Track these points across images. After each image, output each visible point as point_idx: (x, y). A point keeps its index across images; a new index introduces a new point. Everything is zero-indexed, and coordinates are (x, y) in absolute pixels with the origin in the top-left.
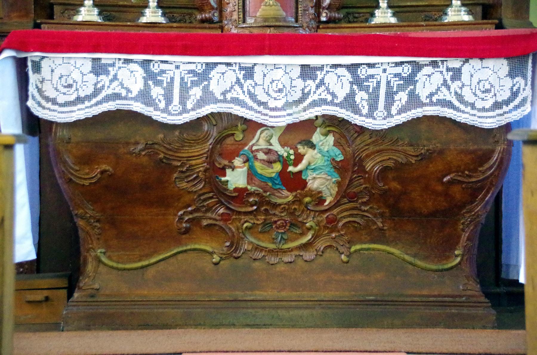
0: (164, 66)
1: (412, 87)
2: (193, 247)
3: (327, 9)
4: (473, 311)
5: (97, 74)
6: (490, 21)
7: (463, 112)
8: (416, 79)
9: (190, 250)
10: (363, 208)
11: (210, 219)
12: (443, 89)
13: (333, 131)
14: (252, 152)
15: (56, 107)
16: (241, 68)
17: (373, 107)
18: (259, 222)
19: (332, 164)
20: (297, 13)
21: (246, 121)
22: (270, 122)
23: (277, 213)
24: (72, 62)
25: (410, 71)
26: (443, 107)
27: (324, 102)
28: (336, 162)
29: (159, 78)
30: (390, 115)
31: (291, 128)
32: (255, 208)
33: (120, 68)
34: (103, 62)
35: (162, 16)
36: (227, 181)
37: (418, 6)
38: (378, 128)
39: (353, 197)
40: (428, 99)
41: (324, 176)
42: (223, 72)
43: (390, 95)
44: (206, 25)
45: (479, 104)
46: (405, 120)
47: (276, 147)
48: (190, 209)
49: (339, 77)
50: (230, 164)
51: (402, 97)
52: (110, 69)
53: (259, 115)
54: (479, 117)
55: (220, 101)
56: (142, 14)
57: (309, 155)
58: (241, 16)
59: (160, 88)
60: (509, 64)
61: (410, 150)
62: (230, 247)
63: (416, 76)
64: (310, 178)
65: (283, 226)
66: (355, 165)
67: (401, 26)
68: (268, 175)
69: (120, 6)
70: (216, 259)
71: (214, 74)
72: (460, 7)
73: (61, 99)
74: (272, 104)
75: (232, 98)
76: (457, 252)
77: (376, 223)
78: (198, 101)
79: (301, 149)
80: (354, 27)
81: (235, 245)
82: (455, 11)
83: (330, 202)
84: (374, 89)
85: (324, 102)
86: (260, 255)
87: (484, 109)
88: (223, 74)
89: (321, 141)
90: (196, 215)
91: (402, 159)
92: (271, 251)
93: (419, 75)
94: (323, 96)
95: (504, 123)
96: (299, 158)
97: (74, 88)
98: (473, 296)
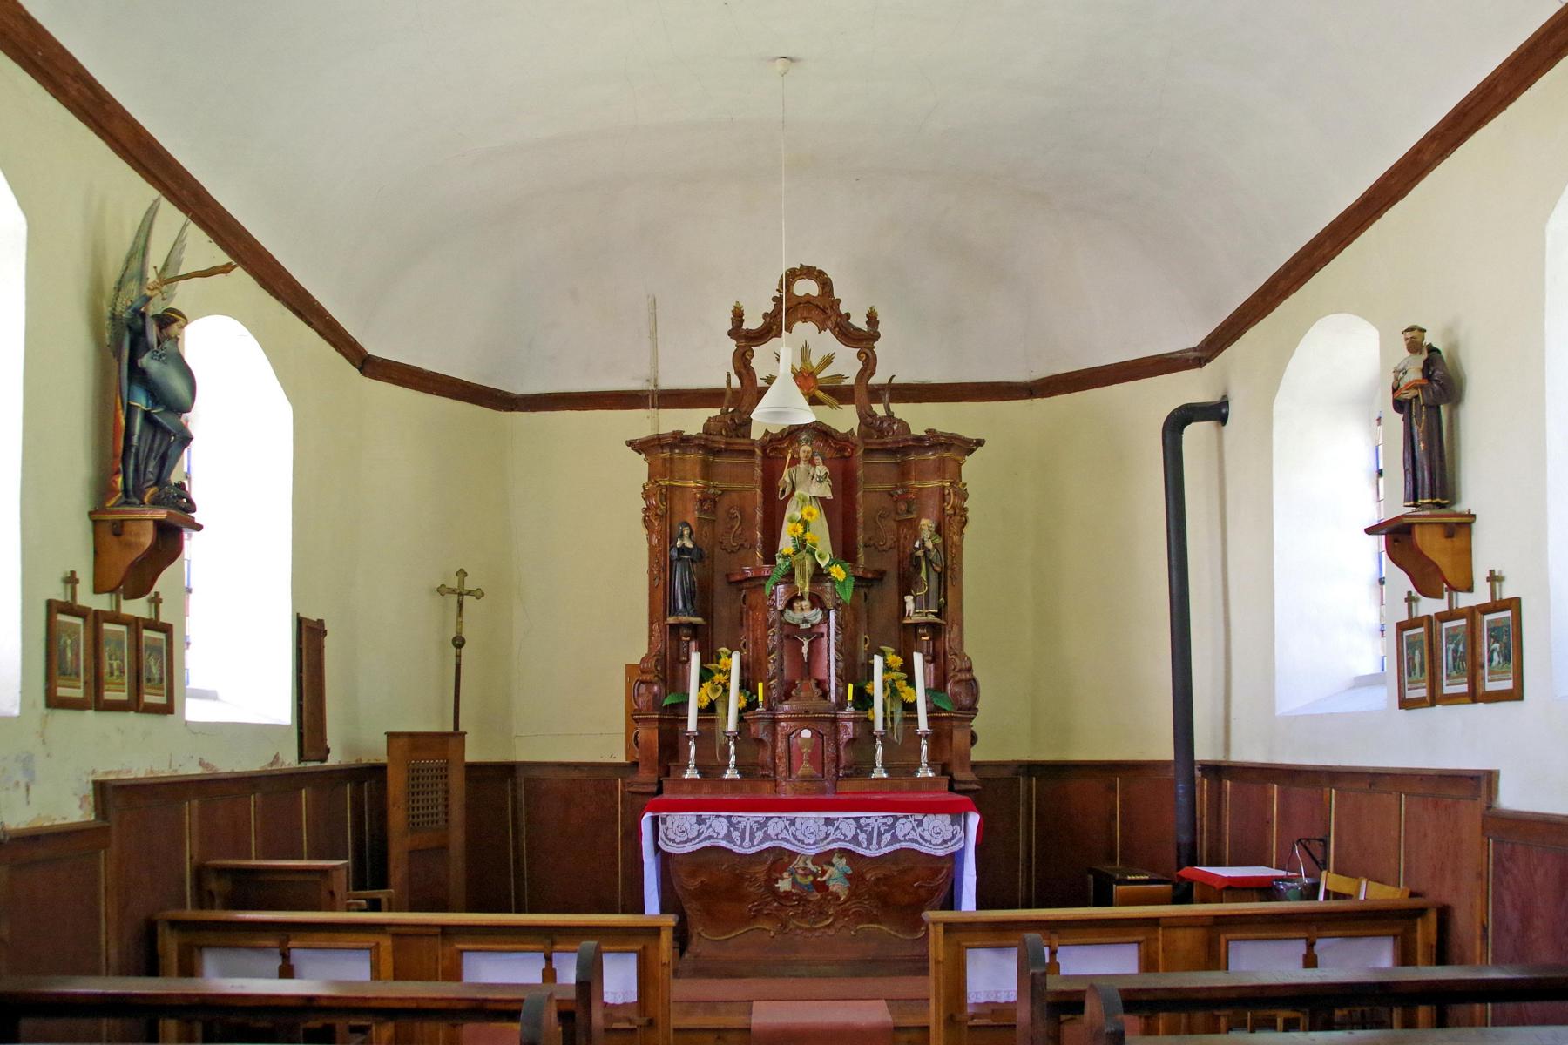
0: (739, 819)
5: (699, 824)
17: (869, 841)
30: (880, 848)
38: (873, 855)
43: (880, 835)
47: (810, 866)
51: (887, 837)
57: (831, 871)
61: (894, 868)
65: (814, 914)
70: (772, 934)
73: (678, 840)
76: (922, 929)
79: (825, 867)
81: (784, 926)
85: (839, 840)
86: (799, 931)
87: (936, 845)
96: (824, 872)
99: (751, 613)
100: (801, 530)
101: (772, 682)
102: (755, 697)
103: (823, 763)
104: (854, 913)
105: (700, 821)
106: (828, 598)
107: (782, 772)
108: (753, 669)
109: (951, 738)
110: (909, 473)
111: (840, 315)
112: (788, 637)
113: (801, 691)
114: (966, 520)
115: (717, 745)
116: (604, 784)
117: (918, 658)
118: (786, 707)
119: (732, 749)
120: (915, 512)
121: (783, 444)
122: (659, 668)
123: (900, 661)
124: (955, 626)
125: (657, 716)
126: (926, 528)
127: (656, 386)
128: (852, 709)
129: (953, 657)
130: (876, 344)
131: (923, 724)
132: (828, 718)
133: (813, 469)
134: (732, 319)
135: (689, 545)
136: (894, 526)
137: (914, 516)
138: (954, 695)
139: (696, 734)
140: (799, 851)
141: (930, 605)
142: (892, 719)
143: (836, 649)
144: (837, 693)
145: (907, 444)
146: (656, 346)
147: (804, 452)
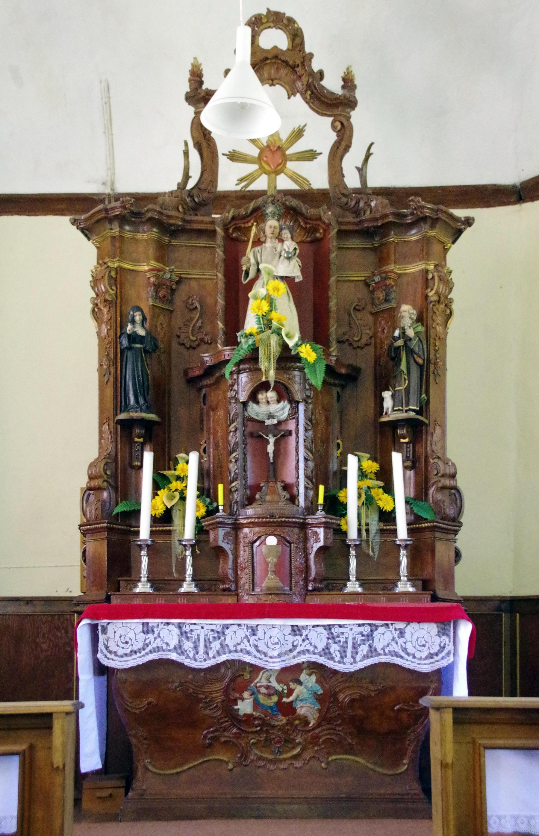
0: (193, 627)
1: (371, 642)
2: (214, 757)
3: (312, 581)
4: (415, 806)
5: (146, 634)
6: (427, 592)
7: (407, 660)
8: (374, 636)
9: (212, 760)
10: (337, 728)
11: (226, 736)
12: (393, 643)
13: (315, 672)
14: (256, 687)
15: (117, 658)
16: (248, 628)
17: (343, 655)
18: (262, 739)
19: (314, 696)
20: (291, 584)
21: (252, 665)
22: (270, 666)
23: (275, 732)
24: (129, 625)
25: (369, 630)
26: (393, 656)
27: (308, 652)
28: (318, 695)
29: (189, 635)
30: (355, 662)
31: (284, 670)
32: (259, 728)
33: (162, 629)
34: (150, 625)
35: (195, 587)
36: (239, 709)
37: (377, 580)
38: (347, 671)
39: (329, 721)
40: (382, 651)
41: (309, 705)
42: (236, 630)
43: (355, 647)
44: (227, 593)
45: (418, 655)
46: (366, 665)
47: (274, 684)
48: (211, 729)
49: (319, 634)
50: (241, 697)
51: (364, 649)
52: (155, 629)
53: (261, 661)
54: (418, 664)
55: (232, 651)
56: (181, 586)
57: (298, 690)
58: (251, 587)
59: (189, 642)
60: (437, 627)
61: (371, 687)
62: (240, 758)
63: (373, 633)
64: (298, 706)
65: (279, 742)
66: (331, 697)
67: (366, 594)
68: (269, 705)
69: (166, 580)
70: (231, 766)
71: (228, 632)
72: (407, 581)
73: (120, 652)
74: (270, 653)
75: (241, 649)
76: (404, 761)
77: (346, 740)
78: (217, 651)
79: (292, 686)
80: (332, 594)
81: (245, 755)
82: (403, 584)
83: (314, 724)
84: (344, 642)
85: (308, 652)
86: (262, 763)
87: (421, 659)
88: (235, 632)
89: (306, 679)
90: (217, 734)
91: (365, 693)
92: (270, 761)
93: (376, 633)
94: (307, 648)
95: (435, 668)
96: (291, 692)
97: (129, 644)
98: (415, 794)
99: (212, 413)
100: (265, 307)
101: (233, 484)
102: (215, 505)
103: (291, 574)
104: (325, 741)
105: (147, 629)
106: (297, 389)
107: (244, 584)
108: (214, 476)
109: (433, 551)
110: (388, 256)
111: (312, 74)
112: (252, 435)
113: (266, 495)
114: (451, 313)
115: (174, 560)
116: (59, 620)
117: (397, 458)
118: (250, 511)
119: (189, 561)
120: (394, 301)
121: (248, 222)
122: (108, 473)
123: (375, 467)
124: (438, 428)
125: (106, 525)
126: (406, 315)
127: (112, 190)
128: (323, 513)
129: (436, 460)
130: (353, 113)
131: (402, 533)
132: (295, 523)
133: (280, 244)
134: (190, 80)
135: (141, 332)
136: (370, 319)
137: (393, 305)
138: (436, 502)
139: (149, 543)
140: (263, 666)
141: (411, 403)
142: (367, 531)
143: (306, 447)
144: (306, 497)
145: (386, 221)
146: (112, 145)
147: (271, 227)
